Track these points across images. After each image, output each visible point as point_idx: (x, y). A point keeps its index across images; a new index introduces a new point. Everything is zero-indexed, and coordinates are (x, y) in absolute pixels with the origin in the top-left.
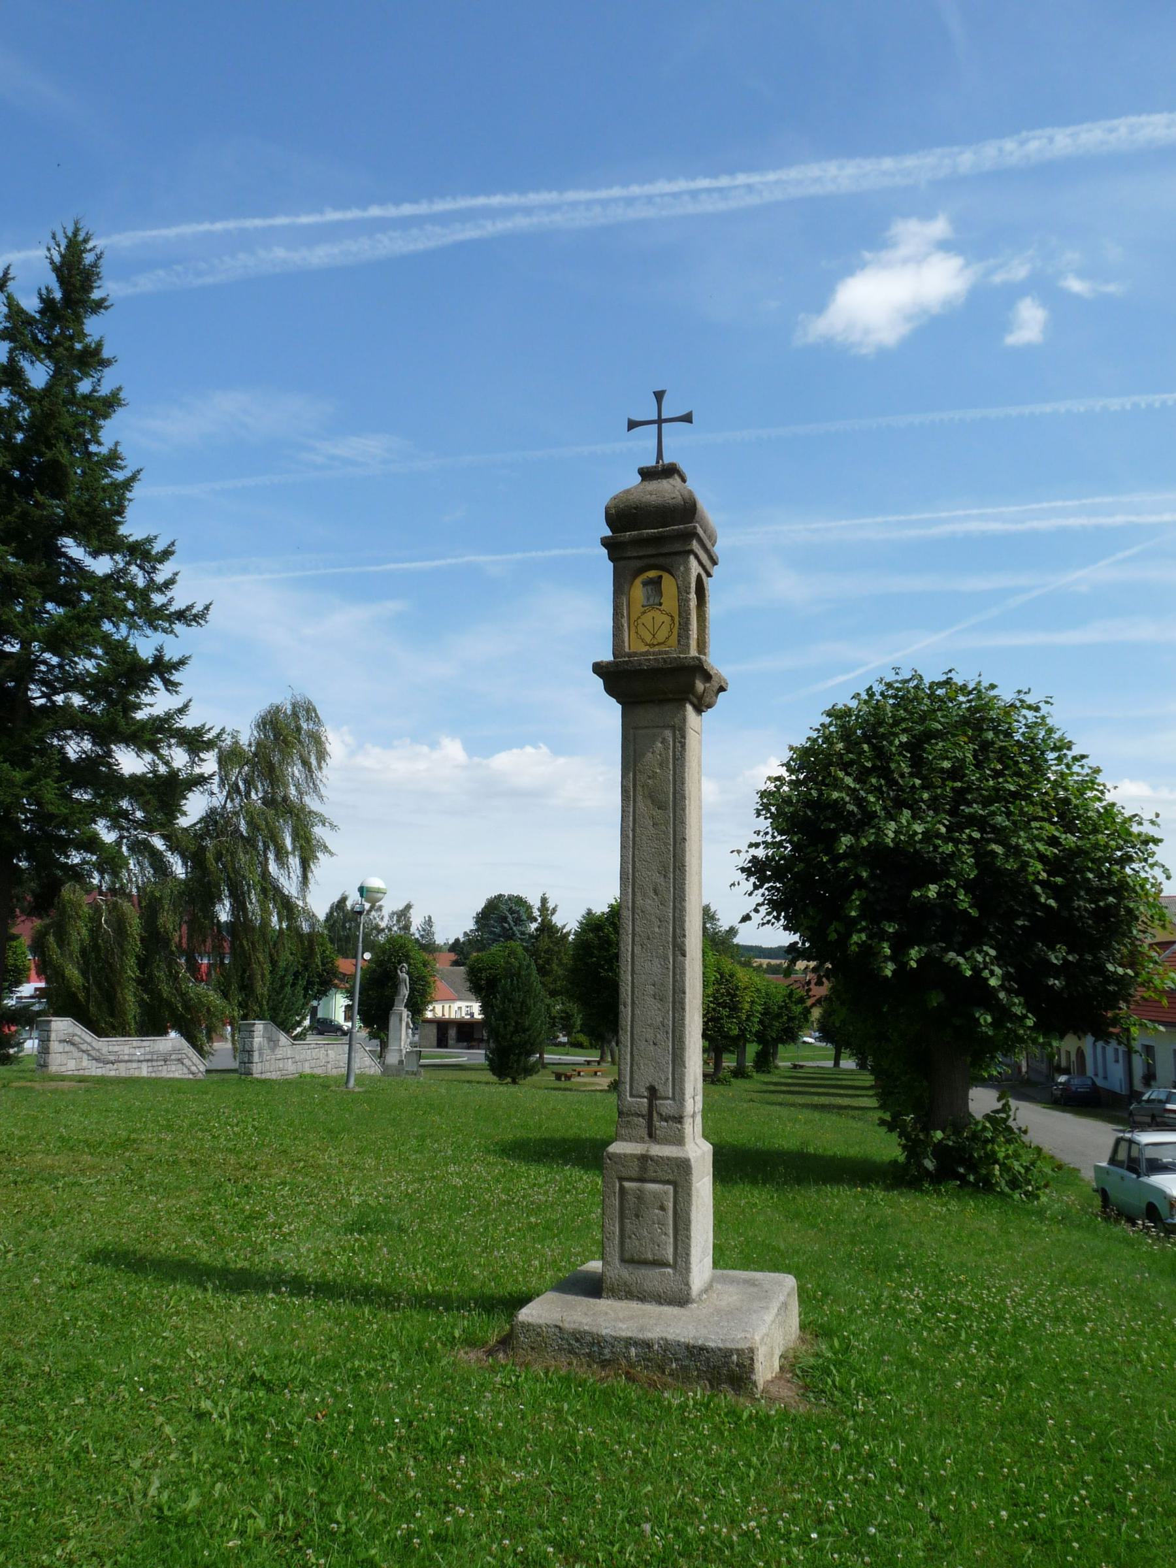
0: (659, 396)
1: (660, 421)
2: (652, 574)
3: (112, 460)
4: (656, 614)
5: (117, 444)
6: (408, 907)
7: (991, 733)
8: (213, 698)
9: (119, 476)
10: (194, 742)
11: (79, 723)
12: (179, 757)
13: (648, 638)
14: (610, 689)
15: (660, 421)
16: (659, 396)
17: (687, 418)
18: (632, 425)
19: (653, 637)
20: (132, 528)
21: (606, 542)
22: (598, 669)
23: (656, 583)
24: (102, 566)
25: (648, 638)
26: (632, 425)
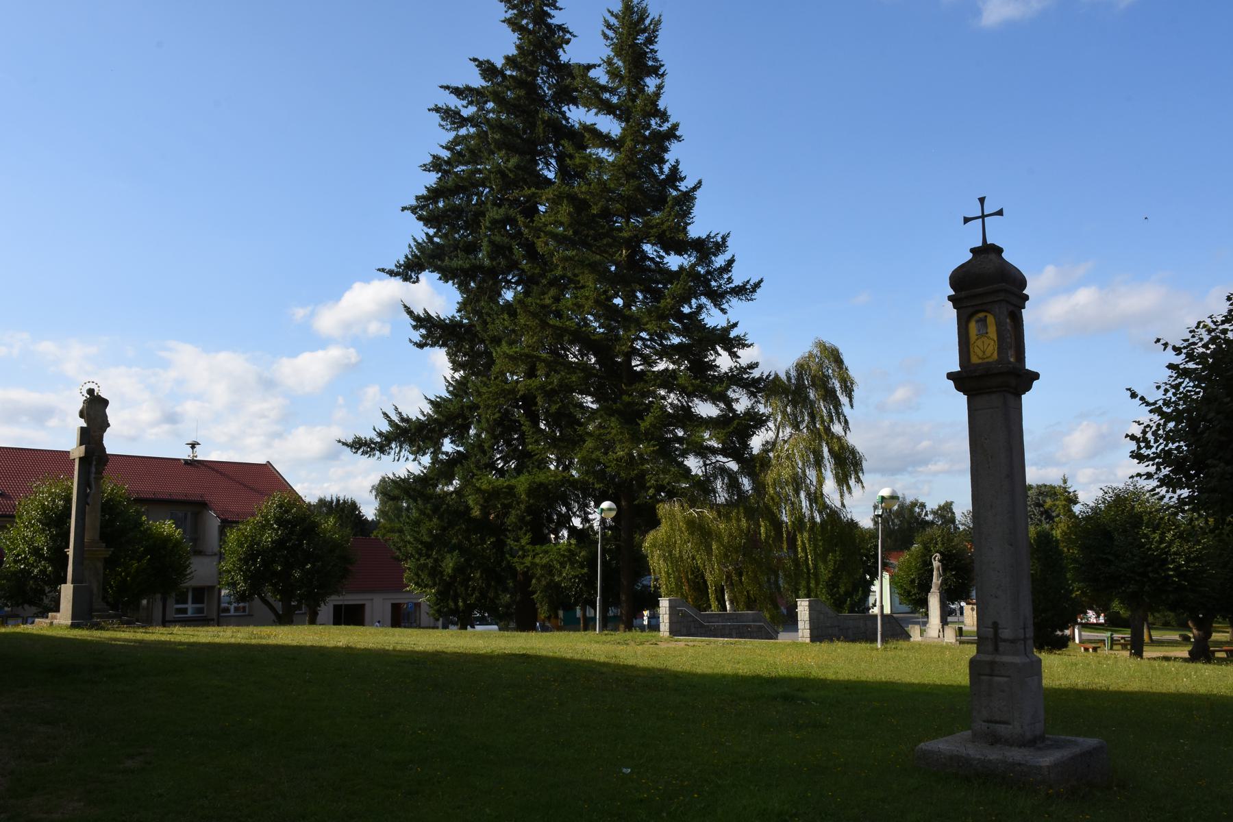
0: (982, 200)
1: (983, 217)
2: (981, 315)
3: (675, 176)
4: (985, 339)
5: (677, 162)
6: (91, 391)
7: (579, 520)
8: (769, 340)
9: (683, 186)
10: (755, 387)
11: (667, 380)
12: (742, 403)
13: (980, 354)
14: (958, 388)
15: (983, 217)
16: (982, 200)
17: (1000, 213)
18: (966, 220)
19: (987, 348)
20: (696, 230)
21: (950, 298)
22: (950, 376)
23: (983, 321)
24: (674, 262)
25: (980, 354)
26: (966, 220)
